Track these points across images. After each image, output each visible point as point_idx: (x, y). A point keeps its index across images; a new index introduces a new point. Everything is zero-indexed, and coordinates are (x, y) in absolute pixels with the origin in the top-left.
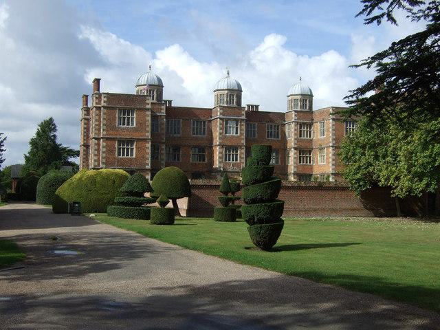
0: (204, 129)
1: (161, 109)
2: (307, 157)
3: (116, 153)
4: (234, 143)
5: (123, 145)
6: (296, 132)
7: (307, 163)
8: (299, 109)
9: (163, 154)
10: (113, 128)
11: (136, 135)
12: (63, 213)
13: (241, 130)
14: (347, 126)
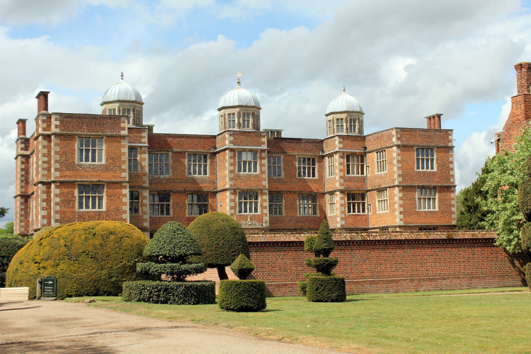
4: (252, 185)
6: (342, 167)
7: (359, 211)
9: (146, 205)
10: (72, 166)
11: (107, 177)
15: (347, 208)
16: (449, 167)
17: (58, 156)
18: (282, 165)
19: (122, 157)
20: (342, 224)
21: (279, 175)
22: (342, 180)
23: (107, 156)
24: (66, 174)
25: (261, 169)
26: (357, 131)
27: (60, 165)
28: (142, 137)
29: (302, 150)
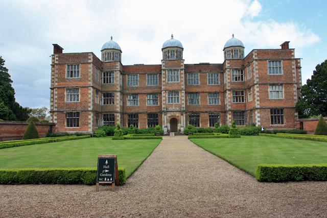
0: (104, 76)
1: (88, 68)
4: (175, 88)
5: (172, 95)
7: (240, 101)
8: (231, 58)
9: (118, 100)
10: (63, 80)
11: (82, 84)
13: (181, 77)
18: (199, 78)
19: (89, 74)
21: (198, 83)
22: (229, 84)
26: (239, 56)
28: (116, 66)
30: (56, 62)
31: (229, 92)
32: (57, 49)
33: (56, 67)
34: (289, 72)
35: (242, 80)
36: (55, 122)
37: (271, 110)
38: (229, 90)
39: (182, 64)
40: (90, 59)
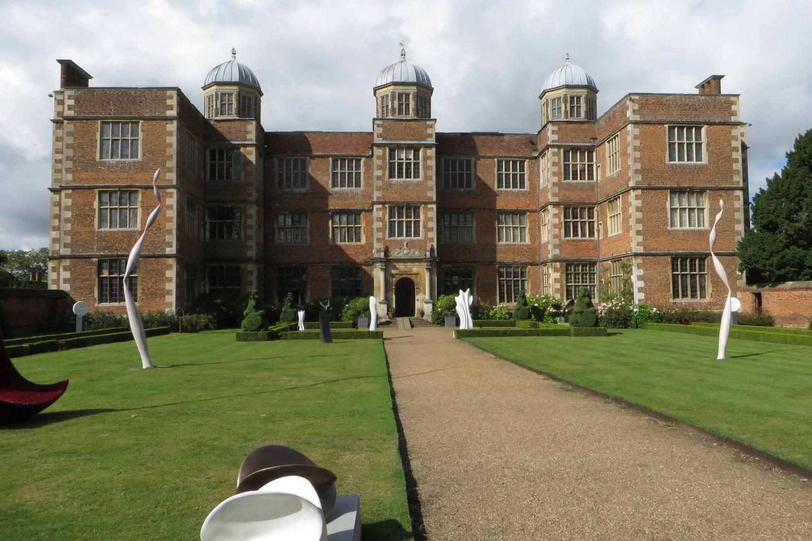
1: (247, 132)
2: (583, 223)
3: (96, 220)
6: (556, 169)
7: (583, 235)
8: (563, 119)
9: (251, 227)
10: (91, 165)
11: (139, 179)
12: (382, 334)
13: (426, 168)
14: (671, 136)
15: (563, 231)
16: (730, 157)
17: (71, 151)
20: (554, 253)
23: (143, 149)
24: (81, 177)
25: (425, 174)
27: (74, 164)
29: (504, 150)
30: (68, 113)
31: (556, 211)
32: (73, 75)
33: (69, 126)
34: (721, 156)
35: (591, 177)
36: (66, 287)
37: (675, 258)
38: (555, 205)
39: (429, 131)
40: (171, 108)
